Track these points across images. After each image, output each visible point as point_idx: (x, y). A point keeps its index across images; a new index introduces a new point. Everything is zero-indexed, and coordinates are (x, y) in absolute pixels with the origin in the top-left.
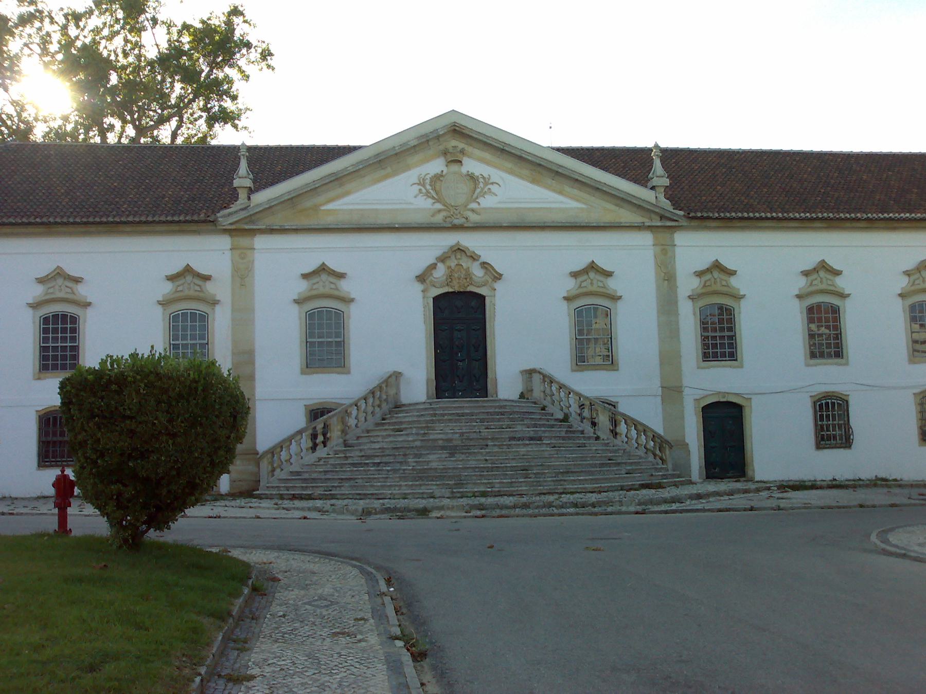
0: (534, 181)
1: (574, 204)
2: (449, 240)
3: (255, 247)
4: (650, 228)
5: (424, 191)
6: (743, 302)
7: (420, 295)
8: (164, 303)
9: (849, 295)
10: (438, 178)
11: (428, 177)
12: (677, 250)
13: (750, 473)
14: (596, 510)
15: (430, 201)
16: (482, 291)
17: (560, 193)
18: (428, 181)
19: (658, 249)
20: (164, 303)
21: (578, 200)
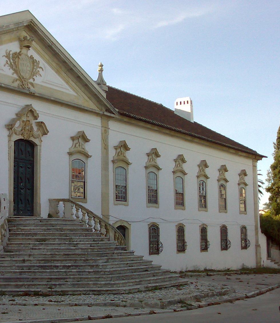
0: (57, 72)
1: (72, 92)
2: (23, 102)
3: (109, 127)
4: (97, 114)
5: (9, 62)
6: (130, 167)
7: (6, 139)
8: (70, 154)
9: (91, 156)
10: (16, 56)
11: (11, 53)
12: (110, 131)
13: (129, 249)
14: (235, 272)
15: (12, 71)
16: (36, 141)
17: (67, 83)
18: (11, 56)
19: (103, 129)
20: (70, 154)
21: (74, 90)
